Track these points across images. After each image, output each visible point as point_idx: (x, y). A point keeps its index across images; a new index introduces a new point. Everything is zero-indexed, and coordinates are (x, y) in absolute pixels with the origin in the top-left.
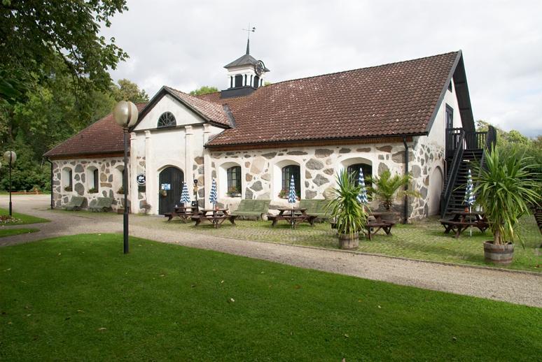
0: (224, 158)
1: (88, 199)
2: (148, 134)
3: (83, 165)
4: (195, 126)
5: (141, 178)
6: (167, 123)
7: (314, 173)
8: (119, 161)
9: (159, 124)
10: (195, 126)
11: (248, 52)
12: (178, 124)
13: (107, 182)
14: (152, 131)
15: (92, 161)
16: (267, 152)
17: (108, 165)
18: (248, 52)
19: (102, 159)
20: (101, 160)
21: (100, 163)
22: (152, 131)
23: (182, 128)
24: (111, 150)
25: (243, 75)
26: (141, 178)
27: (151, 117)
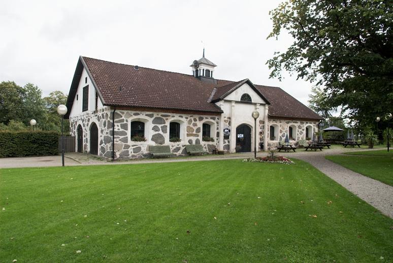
0: (178, 117)
1: (171, 147)
2: (233, 104)
3: (164, 118)
4: (261, 104)
5: (226, 130)
6: (246, 99)
7: (300, 130)
8: (206, 118)
9: (241, 99)
10: (261, 104)
11: (204, 56)
12: (253, 102)
13: (194, 133)
14: (237, 102)
15: (209, 117)
16: (288, 121)
17: (195, 120)
18: (204, 56)
19: (190, 115)
20: (188, 116)
21: (187, 118)
22: (237, 102)
23: (255, 104)
24: (204, 110)
25: (211, 71)
26: (226, 130)
27: (236, 94)
